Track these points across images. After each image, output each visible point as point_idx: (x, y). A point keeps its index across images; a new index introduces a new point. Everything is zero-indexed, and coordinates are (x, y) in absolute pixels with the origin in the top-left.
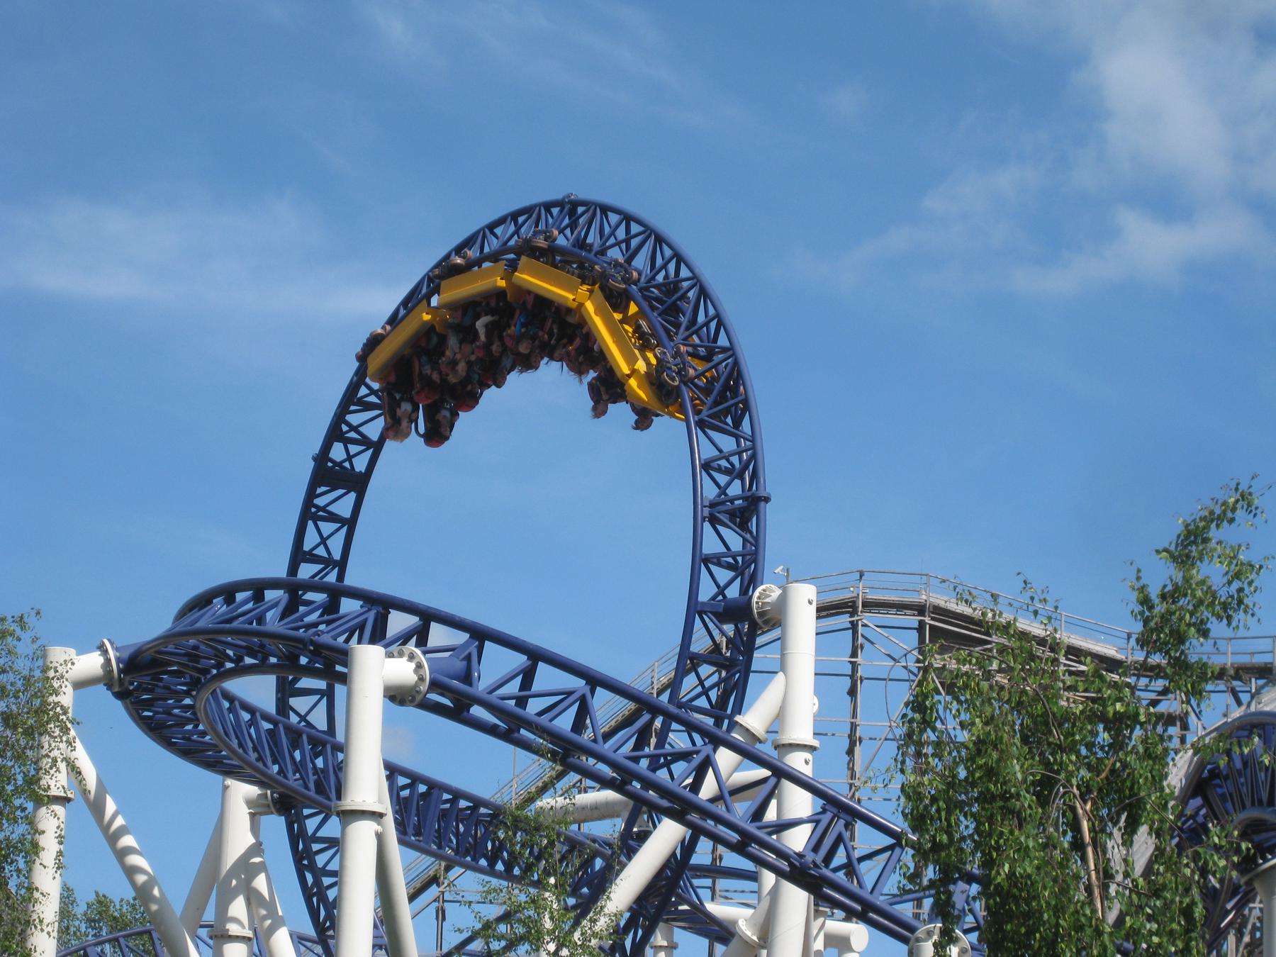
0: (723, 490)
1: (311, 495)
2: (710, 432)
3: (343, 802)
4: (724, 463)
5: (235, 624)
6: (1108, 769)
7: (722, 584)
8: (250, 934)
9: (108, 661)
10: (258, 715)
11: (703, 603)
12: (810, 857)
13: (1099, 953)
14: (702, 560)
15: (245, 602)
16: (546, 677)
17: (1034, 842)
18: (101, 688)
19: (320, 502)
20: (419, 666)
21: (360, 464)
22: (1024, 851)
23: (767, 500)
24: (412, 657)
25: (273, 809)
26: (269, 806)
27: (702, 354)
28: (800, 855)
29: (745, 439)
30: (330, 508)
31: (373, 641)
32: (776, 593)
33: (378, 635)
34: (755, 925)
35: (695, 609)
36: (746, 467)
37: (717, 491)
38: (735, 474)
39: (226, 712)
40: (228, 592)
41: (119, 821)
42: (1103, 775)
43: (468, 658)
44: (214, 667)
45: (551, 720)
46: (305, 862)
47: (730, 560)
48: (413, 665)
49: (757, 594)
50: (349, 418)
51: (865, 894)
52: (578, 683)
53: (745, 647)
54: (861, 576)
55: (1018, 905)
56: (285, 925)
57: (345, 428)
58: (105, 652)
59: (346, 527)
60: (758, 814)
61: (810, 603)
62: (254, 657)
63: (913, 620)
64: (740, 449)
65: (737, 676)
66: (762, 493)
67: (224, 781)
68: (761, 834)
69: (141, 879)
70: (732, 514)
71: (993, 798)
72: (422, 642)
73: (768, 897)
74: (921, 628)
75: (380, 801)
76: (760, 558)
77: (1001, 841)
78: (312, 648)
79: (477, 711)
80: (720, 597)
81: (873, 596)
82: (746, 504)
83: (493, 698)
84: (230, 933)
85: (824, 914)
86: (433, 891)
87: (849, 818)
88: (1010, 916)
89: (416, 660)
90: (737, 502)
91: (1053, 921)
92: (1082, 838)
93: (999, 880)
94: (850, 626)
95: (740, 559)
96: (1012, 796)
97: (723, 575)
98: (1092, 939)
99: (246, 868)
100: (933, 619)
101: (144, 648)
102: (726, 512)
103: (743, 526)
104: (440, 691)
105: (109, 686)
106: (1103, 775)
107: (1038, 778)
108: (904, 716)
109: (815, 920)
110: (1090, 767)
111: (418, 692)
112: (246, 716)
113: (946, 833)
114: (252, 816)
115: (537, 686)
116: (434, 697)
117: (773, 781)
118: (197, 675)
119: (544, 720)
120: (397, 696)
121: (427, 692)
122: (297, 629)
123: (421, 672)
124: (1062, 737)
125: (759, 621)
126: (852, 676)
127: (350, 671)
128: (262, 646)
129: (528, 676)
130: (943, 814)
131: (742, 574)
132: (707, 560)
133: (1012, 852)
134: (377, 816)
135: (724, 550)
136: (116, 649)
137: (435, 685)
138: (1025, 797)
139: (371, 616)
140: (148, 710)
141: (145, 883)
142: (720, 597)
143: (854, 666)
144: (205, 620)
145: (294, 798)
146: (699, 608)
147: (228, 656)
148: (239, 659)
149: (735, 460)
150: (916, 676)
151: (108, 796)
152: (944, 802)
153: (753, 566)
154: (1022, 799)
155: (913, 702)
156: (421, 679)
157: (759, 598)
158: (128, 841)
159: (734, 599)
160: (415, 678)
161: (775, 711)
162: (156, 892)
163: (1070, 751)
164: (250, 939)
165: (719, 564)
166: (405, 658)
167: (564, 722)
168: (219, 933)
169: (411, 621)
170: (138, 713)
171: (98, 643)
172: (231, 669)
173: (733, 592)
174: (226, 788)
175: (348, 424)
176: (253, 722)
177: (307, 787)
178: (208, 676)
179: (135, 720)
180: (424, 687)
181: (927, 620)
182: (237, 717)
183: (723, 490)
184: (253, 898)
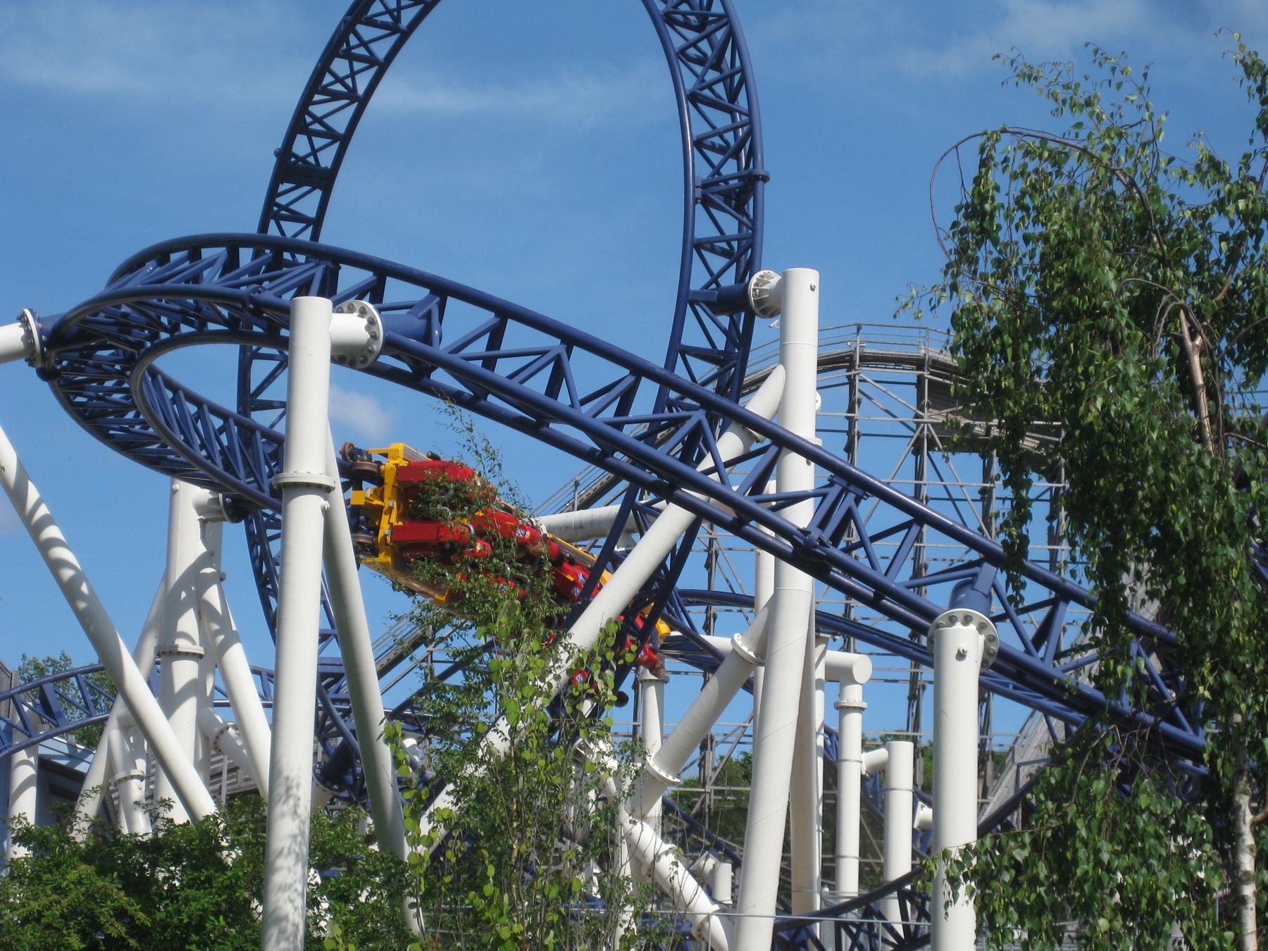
0: (717, 170)
1: (273, 193)
2: (701, 106)
3: (285, 474)
4: (717, 141)
5: (168, 284)
6: (1225, 289)
7: (715, 271)
8: (199, 649)
9: (29, 333)
10: (205, 407)
11: (695, 293)
12: (815, 534)
13: (1223, 517)
14: (694, 246)
15: (181, 261)
16: (517, 336)
17: (1135, 368)
18: (22, 363)
19: (282, 200)
20: (372, 322)
21: (326, 159)
22: (1122, 382)
23: (765, 179)
24: (363, 312)
25: (225, 515)
26: (220, 512)
27: (694, 23)
28: (805, 532)
29: (741, 113)
30: (292, 207)
31: (321, 293)
32: (775, 279)
33: (328, 289)
34: (752, 640)
35: (686, 299)
36: (741, 145)
37: (709, 170)
38: (729, 152)
39: (169, 403)
40: (160, 254)
41: (43, 511)
42: (1220, 297)
43: (428, 316)
44: (148, 339)
45: (522, 382)
46: (269, 586)
47: (724, 245)
48: (364, 322)
49: (754, 280)
50: (312, 109)
51: (878, 576)
52: (552, 343)
53: (741, 340)
54: (858, 330)
55: (1112, 454)
56: (239, 641)
57: (308, 119)
58: (25, 323)
59: (311, 227)
60: (758, 486)
61: (812, 289)
62: (190, 324)
63: (911, 375)
64: (735, 125)
65: (733, 370)
66: (760, 171)
67: (172, 483)
68: (762, 509)
69: (67, 574)
70: (727, 195)
71: (1078, 314)
72: (377, 297)
73: (766, 609)
74: (919, 383)
75: (328, 473)
76: (758, 241)
77: (1091, 369)
78: (251, 306)
79: (440, 376)
80: (714, 286)
81: (870, 350)
82: (742, 183)
83: (456, 359)
84: (180, 649)
85: (825, 641)
86: (421, 652)
87: (860, 492)
88: (1103, 468)
89: (368, 316)
90: (731, 182)
91: (1162, 474)
92: (1192, 380)
93: (1090, 418)
94: (847, 381)
95: (735, 244)
96: (1103, 312)
97: (717, 262)
98: (1213, 498)
99: (195, 579)
100: (932, 374)
101: (69, 316)
102: (719, 193)
103: (739, 208)
104: (396, 352)
105: (31, 362)
106: (1220, 297)
107: (1136, 294)
108: (955, 224)
109: (816, 646)
110: (1202, 287)
111: (371, 352)
112: (193, 409)
113: (1013, 376)
114: (203, 523)
115: (506, 345)
116: (388, 360)
117: (773, 450)
118: (130, 350)
119: (514, 384)
120: (345, 356)
121: (381, 353)
122: (238, 286)
123: (374, 329)
124: (1165, 247)
125: (757, 310)
126: (850, 432)
127: (292, 333)
128: (198, 309)
129: (496, 334)
130: (1009, 352)
131: (738, 261)
132: (699, 246)
133: (1105, 382)
134: (324, 490)
135: (717, 234)
136: (38, 320)
137: (391, 346)
138: (1121, 312)
139: (319, 272)
140: (81, 395)
141: (72, 579)
142: (714, 286)
143: (851, 421)
144: (135, 282)
145: (250, 502)
146: (690, 298)
147: (162, 325)
148: (174, 328)
149: (729, 136)
150: (915, 432)
151: (30, 483)
152: (1010, 335)
153: (750, 251)
154: (1118, 316)
155: (967, 206)
156: (374, 337)
157: (756, 284)
158: (52, 532)
159: (729, 289)
160: (366, 336)
161: (778, 399)
162: (84, 588)
163: (1175, 265)
164: (201, 656)
165: (713, 250)
166: (356, 314)
167: (537, 385)
168: (167, 650)
169: (365, 276)
170: (68, 398)
171: (19, 314)
172: (167, 341)
173: (728, 280)
174: (174, 492)
175: (311, 115)
176: (199, 416)
177: (261, 489)
178: (142, 351)
179: (66, 408)
180: (377, 347)
181: (926, 374)
182: (182, 409)
183: (717, 170)
184: (204, 612)
